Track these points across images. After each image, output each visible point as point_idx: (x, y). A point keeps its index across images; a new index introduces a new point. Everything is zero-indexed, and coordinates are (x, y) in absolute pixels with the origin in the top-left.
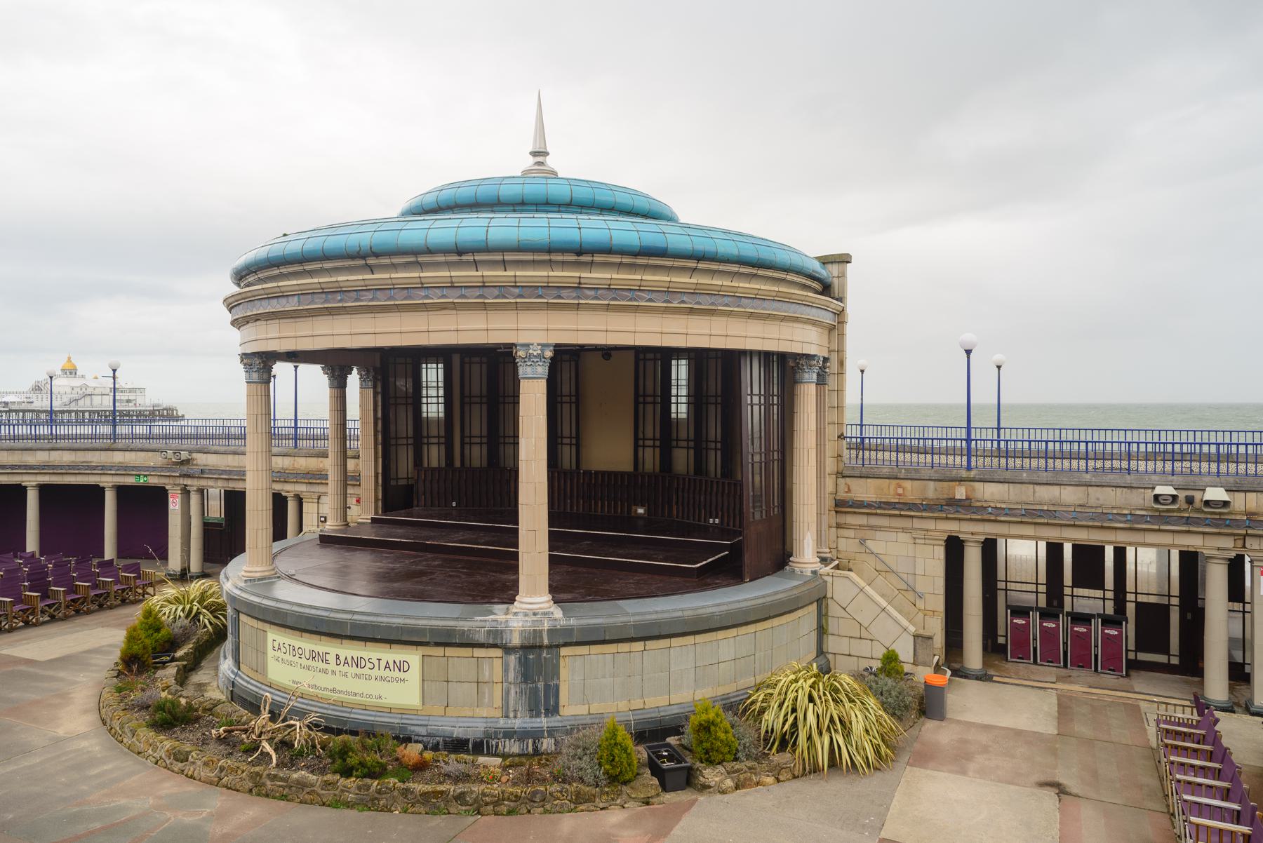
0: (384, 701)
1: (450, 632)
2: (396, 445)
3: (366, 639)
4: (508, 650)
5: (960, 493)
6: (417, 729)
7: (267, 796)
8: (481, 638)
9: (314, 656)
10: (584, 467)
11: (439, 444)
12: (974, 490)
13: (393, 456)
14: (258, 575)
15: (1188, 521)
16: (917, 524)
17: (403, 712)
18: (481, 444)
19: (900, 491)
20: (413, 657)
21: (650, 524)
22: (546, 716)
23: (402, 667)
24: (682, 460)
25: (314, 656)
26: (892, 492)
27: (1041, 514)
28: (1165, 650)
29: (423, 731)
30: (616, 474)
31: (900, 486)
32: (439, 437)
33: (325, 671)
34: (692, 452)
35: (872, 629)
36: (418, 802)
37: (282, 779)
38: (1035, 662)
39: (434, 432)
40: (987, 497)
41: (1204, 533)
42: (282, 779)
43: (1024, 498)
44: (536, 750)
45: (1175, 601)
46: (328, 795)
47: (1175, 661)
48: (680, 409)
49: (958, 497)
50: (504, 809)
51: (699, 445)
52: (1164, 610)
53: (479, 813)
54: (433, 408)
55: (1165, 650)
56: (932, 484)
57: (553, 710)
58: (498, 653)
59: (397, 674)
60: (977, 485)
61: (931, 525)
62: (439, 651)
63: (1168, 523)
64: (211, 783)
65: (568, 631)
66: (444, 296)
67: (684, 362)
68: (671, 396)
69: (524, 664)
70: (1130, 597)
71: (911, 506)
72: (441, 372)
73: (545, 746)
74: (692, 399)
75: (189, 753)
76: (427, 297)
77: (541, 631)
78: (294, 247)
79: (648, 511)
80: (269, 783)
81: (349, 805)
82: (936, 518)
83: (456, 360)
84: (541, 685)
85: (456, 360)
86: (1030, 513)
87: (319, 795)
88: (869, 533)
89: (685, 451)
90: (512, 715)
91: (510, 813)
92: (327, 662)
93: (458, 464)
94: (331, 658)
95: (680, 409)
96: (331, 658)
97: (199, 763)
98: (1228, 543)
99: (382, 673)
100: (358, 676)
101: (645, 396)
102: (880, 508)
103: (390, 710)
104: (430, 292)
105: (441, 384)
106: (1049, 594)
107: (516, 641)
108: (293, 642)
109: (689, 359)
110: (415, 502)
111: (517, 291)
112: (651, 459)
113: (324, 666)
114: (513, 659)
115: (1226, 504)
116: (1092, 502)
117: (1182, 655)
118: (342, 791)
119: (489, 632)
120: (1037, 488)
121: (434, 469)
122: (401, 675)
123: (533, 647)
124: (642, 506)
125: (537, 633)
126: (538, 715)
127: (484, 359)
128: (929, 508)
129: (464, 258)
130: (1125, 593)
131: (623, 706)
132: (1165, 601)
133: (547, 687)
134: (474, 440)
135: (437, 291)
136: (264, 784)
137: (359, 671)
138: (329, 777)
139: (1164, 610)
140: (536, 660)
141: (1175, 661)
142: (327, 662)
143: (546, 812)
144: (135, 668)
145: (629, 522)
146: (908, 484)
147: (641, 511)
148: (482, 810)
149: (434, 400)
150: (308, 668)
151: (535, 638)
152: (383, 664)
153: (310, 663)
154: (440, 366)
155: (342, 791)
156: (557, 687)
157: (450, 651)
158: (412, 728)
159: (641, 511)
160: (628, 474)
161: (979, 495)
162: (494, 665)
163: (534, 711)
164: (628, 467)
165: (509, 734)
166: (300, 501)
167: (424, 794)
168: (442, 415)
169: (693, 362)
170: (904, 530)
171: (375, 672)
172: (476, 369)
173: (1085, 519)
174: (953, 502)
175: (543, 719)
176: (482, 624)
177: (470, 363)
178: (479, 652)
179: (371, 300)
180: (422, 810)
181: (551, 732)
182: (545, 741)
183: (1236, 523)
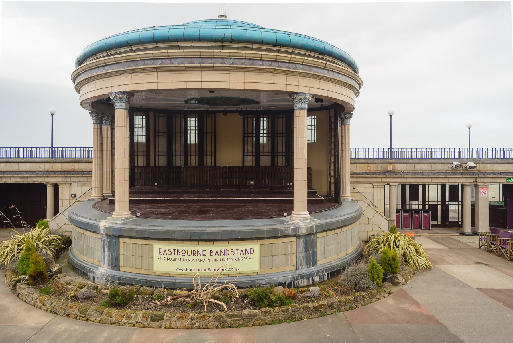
0: (239, 270)
1: (276, 231)
2: (278, 155)
3: (243, 239)
4: (298, 236)
5: (390, 168)
6: (261, 281)
7: (230, 327)
8: (290, 232)
9: (194, 253)
10: (217, 165)
11: (143, 155)
12: (395, 166)
13: (276, 141)
14: (126, 216)
15: (462, 174)
16: (375, 180)
17: (250, 274)
18: (164, 155)
19: (369, 168)
20: (256, 246)
21: (255, 187)
22: (313, 266)
23: (249, 252)
24: (265, 161)
25: (194, 253)
26: (366, 168)
27: (418, 173)
28: (437, 220)
29: (263, 282)
30: (236, 167)
31: (369, 166)
32: (143, 152)
33: (203, 260)
34: (270, 157)
35: (373, 220)
36: (313, 312)
37: (238, 316)
38: (402, 228)
39: (140, 149)
40: (399, 169)
41: (465, 178)
42: (238, 316)
43: (411, 169)
44: (313, 282)
45: (440, 203)
46: (267, 318)
47: (439, 223)
48: (264, 139)
49: (389, 169)
50: (348, 307)
51: (273, 154)
52: (437, 206)
53: (340, 312)
54: (140, 138)
55: (437, 220)
56: (380, 165)
57: (315, 263)
58: (294, 239)
59: (247, 255)
60: (396, 164)
61: (380, 180)
62: (268, 241)
63: (456, 175)
64: (188, 328)
65: (321, 226)
66: (270, 65)
67: (265, 119)
68: (260, 133)
69: (306, 243)
70: (427, 203)
71: (374, 173)
72: (144, 120)
73: (316, 280)
74: (270, 135)
75: (163, 315)
76: (262, 65)
77: (313, 226)
78: (160, 33)
79: (255, 183)
80: (228, 320)
81: (281, 321)
82: (382, 177)
83: (151, 114)
84: (311, 252)
85: (151, 114)
86: (414, 173)
87: (262, 320)
88: (356, 185)
89: (266, 157)
90: (300, 268)
91: (351, 308)
92: (204, 255)
93: (152, 164)
94: (207, 253)
95: (264, 139)
96: (207, 253)
97: (173, 319)
98: (472, 180)
99: (239, 256)
100: (224, 260)
101: (247, 133)
102: (362, 175)
103: (243, 275)
104: (264, 63)
105: (144, 126)
106: (402, 204)
107: (304, 232)
108: (177, 248)
109: (268, 118)
110: (136, 184)
111: (302, 66)
112: (250, 161)
113: (202, 257)
114: (301, 241)
115: (475, 167)
116: (433, 169)
117: (441, 221)
118: (275, 315)
119: (293, 229)
120: (416, 165)
121: (141, 167)
122: (250, 256)
123: (310, 234)
124: (252, 180)
125: (312, 227)
126: (310, 266)
127: (165, 115)
128: (379, 174)
129: (276, 48)
130: (425, 201)
131: (336, 257)
132: (436, 203)
133: (313, 252)
134: (160, 154)
135: (267, 62)
136: (226, 321)
137: (225, 257)
138: (264, 309)
139: (437, 206)
140: (309, 240)
141: (439, 223)
142: (204, 255)
143: (362, 305)
144: (39, 280)
145: (249, 186)
146: (371, 165)
147: (252, 183)
148: (341, 309)
149: (139, 134)
150: (190, 260)
151: (311, 230)
152: (239, 252)
153: (192, 257)
154: (144, 117)
155: (275, 315)
156: (316, 252)
157: (274, 241)
158: (258, 281)
159: (252, 183)
160: (239, 167)
161: (396, 168)
162: (292, 245)
163: (309, 265)
164: (240, 164)
165: (302, 277)
166: (56, 187)
167: (315, 308)
168: (144, 141)
169: (270, 119)
170: (370, 183)
171: (235, 256)
172: (161, 119)
173: (432, 175)
174: (388, 171)
175: (313, 268)
176: (288, 226)
177: (159, 116)
178: (287, 240)
179: (232, 64)
180: (316, 315)
181: (318, 272)
182: (316, 277)
183: (474, 174)
